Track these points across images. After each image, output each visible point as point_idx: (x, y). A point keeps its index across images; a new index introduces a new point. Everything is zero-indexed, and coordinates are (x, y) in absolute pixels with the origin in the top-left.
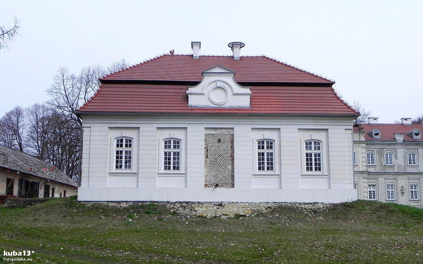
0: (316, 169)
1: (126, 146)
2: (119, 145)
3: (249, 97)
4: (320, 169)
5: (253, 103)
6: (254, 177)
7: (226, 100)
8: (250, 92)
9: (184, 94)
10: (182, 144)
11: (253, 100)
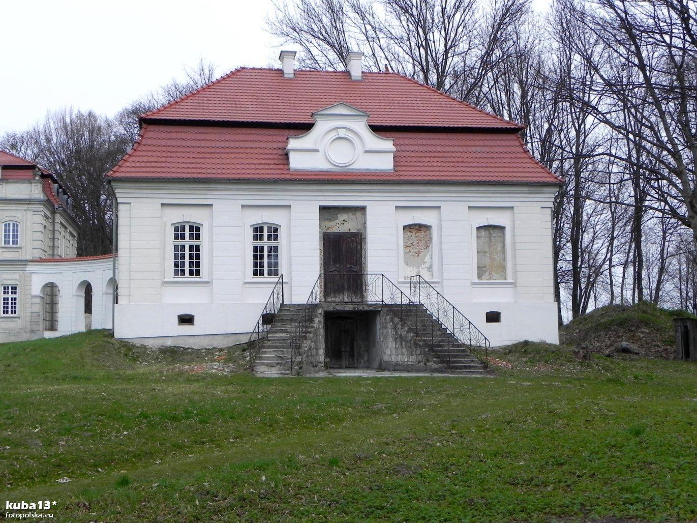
0: (191, 273)
1: (269, 238)
2: (179, 236)
3: (392, 156)
4: (276, 274)
5: (399, 169)
6: (473, 286)
7: (354, 160)
8: (394, 149)
9: (281, 152)
10: (282, 233)
11: (398, 164)
